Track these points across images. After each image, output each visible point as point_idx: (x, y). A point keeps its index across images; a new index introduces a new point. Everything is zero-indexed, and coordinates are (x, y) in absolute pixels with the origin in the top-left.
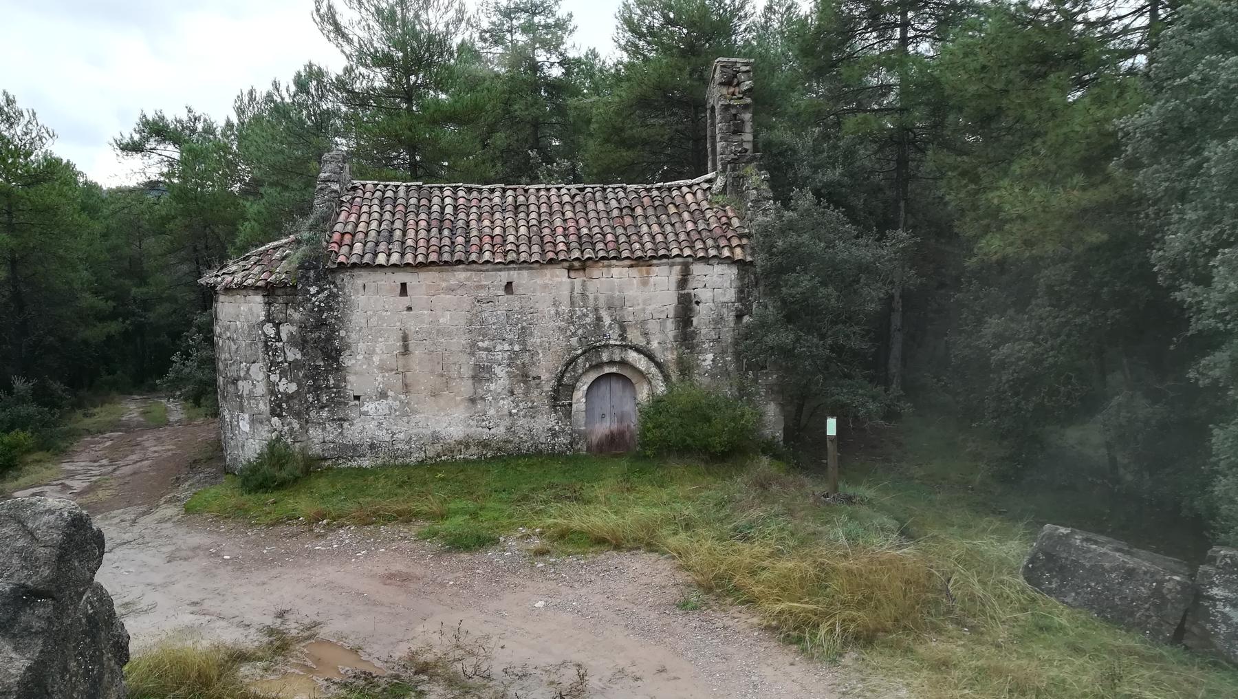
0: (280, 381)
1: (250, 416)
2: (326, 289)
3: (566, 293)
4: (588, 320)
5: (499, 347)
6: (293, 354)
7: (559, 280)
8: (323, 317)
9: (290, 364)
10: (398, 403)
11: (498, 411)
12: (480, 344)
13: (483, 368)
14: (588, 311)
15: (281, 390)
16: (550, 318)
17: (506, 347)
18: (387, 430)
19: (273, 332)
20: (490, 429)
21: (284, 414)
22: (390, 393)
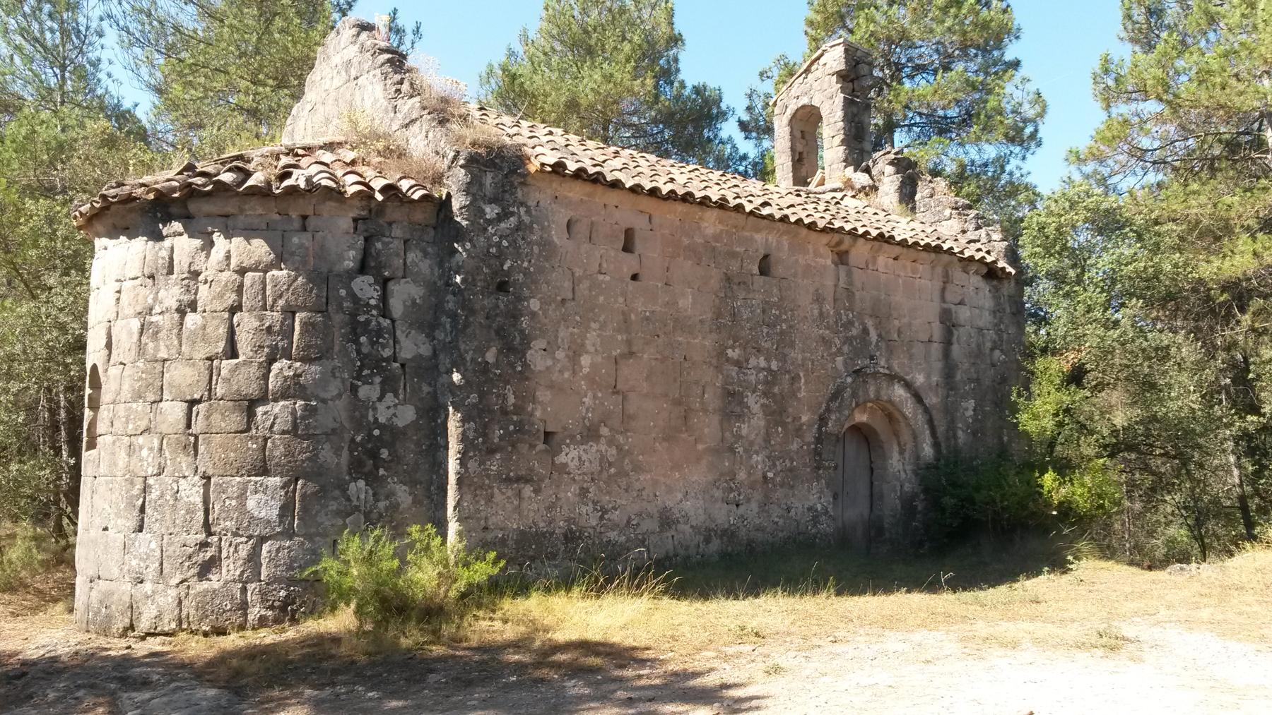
0: (380, 399)
2: (512, 214)
4: (854, 332)
8: (505, 267)
9: (403, 365)
10: (614, 452)
11: (749, 474)
15: (382, 420)
16: (813, 321)
18: (595, 503)
19: (375, 294)
21: (382, 472)
22: (604, 431)
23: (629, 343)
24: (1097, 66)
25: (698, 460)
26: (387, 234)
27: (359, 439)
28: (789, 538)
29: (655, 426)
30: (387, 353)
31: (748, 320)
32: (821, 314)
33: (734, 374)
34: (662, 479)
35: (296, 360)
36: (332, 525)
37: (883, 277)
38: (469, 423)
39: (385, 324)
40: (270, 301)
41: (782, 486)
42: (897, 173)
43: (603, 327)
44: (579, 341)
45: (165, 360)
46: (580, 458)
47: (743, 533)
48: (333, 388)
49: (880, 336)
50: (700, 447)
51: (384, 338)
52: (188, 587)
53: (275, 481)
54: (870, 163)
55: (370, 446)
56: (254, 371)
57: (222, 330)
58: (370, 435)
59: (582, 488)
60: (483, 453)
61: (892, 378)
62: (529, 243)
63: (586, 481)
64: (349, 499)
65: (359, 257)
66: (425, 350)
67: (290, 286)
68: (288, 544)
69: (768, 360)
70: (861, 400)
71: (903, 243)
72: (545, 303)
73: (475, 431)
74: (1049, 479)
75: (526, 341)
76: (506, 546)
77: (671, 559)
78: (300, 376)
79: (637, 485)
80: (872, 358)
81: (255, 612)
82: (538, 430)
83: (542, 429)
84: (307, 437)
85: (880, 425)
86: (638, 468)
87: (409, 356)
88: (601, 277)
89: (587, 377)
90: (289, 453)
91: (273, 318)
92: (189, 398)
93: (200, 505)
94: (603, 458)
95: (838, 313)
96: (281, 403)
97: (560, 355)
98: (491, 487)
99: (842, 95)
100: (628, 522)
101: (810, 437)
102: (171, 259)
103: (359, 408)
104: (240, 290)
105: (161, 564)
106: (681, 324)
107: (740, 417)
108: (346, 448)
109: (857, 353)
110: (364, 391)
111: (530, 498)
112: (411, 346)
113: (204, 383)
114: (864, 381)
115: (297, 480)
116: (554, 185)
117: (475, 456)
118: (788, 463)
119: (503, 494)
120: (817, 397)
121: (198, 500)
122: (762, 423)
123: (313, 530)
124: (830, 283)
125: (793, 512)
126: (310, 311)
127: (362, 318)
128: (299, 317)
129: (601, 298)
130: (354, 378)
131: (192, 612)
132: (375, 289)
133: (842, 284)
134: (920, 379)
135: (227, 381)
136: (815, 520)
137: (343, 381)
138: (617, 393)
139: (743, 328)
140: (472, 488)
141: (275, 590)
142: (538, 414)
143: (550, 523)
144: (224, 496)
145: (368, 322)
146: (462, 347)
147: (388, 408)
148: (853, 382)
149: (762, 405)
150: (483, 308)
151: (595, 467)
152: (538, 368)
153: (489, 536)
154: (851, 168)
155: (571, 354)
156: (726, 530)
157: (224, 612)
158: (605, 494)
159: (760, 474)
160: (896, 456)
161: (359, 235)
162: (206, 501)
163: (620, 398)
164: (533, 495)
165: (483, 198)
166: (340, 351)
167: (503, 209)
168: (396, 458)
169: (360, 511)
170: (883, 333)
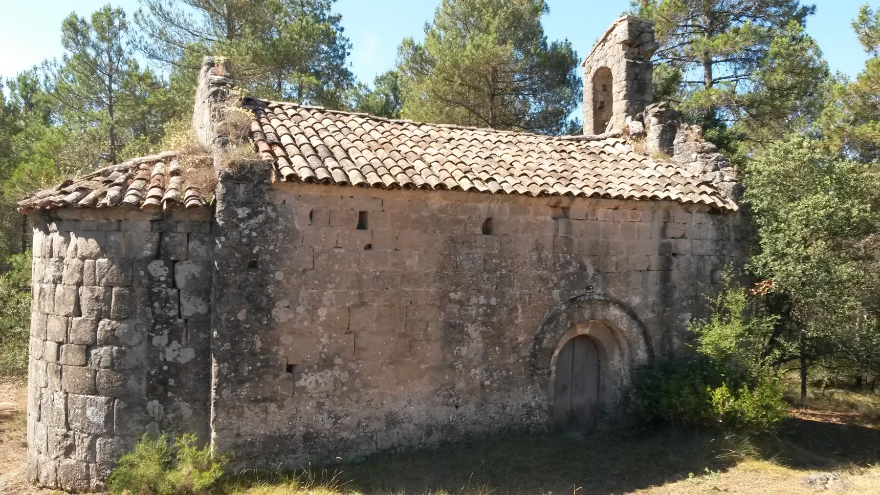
0: (168, 345)
2: (261, 212)
4: (572, 269)
8: (254, 251)
10: (346, 375)
11: (468, 384)
15: (169, 359)
16: (532, 265)
18: (329, 412)
19: (165, 273)
21: (170, 394)
22: (338, 361)
23: (361, 295)
24: (856, 16)
25: (421, 376)
26: (175, 230)
27: (153, 372)
28: (504, 428)
29: (382, 355)
30: (172, 313)
32: (540, 259)
33: (456, 311)
34: (389, 392)
35: (113, 319)
36: (137, 430)
37: (602, 225)
38: (223, 363)
39: (172, 294)
40: (97, 281)
41: (498, 391)
42: (660, 123)
44: (317, 298)
45: (48, 314)
46: (317, 382)
47: (461, 428)
48: (136, 339)
49: (597, 270)
50: (423, 367)
51: (170, 303)
52: (60, 461)
53: (102, 399)
54: (644, 114)
55: (161, 377)
56: (88, 326)
57: (72, 298)
58: (161, 369)
59: (318, 403)
60: (235, 384)
61: (607, 302)
62: (274, 232)
63: (322, 398)
64: (147, 413)
65: (155, 247)
66: (202, 309)
67: (109, 269)
68: (110, 440)
69: (488, 297)
71: (619, 197)
72: (288, 274)
73: (229, 369)
74: (719, 394)
75: (272, 303)
76: (255, 447)
77: (396, 448)
78: (115, 330)
79: (367, 398)
80: (588, 288)
81: (94, 482)
82: (281, 365)
83: (285, 363)
84: (120, 371)
85: (601, 335)
87: (189, 314)
88: (337, 250)
89: (322, 324)
90: (109, 381)
91: (100, 290)
92: (57, 341)
93: (63, 410)
94: (336, 381)
95: (556, 257)
96: (104, 348)
97: (301, 309)
98: (242, 407)
99: (626, 60)
100: (359, 424)
101: (525, 353)
102: (51, 247)
103: (153, 352)
104: (81, 271)
105: (47, 445)
106: (407, 278)
107: (460, 342)
108: (145, 379)
109: (573, 286)
110: (156, 340)
112: (191, 307)
113: (64, 332)
114: (579, 307)
115: (115, 398)
116: (295, 188)
118: (504, 373)
119: (252, 411)
120: (533, 323)
121: (62, 407)
122: (481, 345)
123: (125, 432)
124: (549, 234)
126: (121, 286)
127: (156, 290)
128: (115, 290)
130: (149, 331)
131: (62, 477)
132: (165, 270)
133: (561, 233)
134: (636, 300)
135: (75, 331)
136: (529, 414)
137: (142, 333)
138: (350, 333)
139: (464, 276)
140: (226, 409)
141: (104, 469)
142: (281, 353)
143: (292, 428)
144: (75, 406)
145: (160, 292)
146: (219, 310)
147: (174, 351)
148: (567, 309)
149: (481, 332)
150: (235, 282)
151: (330, 387)
152: (281, 321)
153: (240, 441)
154: (630, 118)
155: (310, 308)
156: (446, 426)
157: (78, 479)
158: (339, 406)
159: (477, 383)
160: (617, 357)
161: (155, 232)
162: (66, 409)
163: (352, 336)
165: (236, 203)
166: (141, 313)
167: (253, 210)
168: (180, 385)
169: (155, 421)
170: (601, 268)
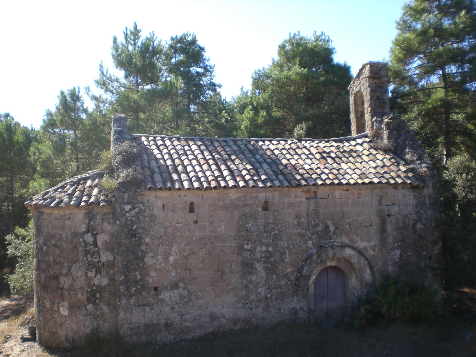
1: (69, 303)
2: (136, 207)
3: (304, 208)
4: (320, 228)
5: (258, 249)
6: (304, 242)
7: (300, 199)
8: (134, 228)
12: (245, 247)
13: (247, 265)
14: (319, 221)
15: (96, 284)
17: (264, 248)
18: (178, 312)
20: (251, 310)
21: (97, 301)
22: (181, 285)
27: (89, 290)
31: (255, 232)
43: (179, 244)
46: (170, 296)
51: (95, 255)
58: (92, 289)
62: (144, 217)
66: (111, 258)
70: (324, 259)
82: (151, 287)
86: (197, 298)
87: (105, 261)
88: (178, 225)
94: (181, 295)
97: (160, 257)
98: (132, 309)
107: (251, 273)
110: (90, 274)
111: (148, 312)
117: (124, 298)
118: (279, 290)
119: (137, 311)
122: (264, 274)
125: (282, 311)
129: (178, 234)
133: (312, 208)
138: (187, 269)
143: (158, 320)
145: (90, 249)
149: (264, 267)
151: (178, 298)
155: (165, 256)
163: (188, 271)
164: (150, 311)
165: (124, 203)
167: (132, 206)
